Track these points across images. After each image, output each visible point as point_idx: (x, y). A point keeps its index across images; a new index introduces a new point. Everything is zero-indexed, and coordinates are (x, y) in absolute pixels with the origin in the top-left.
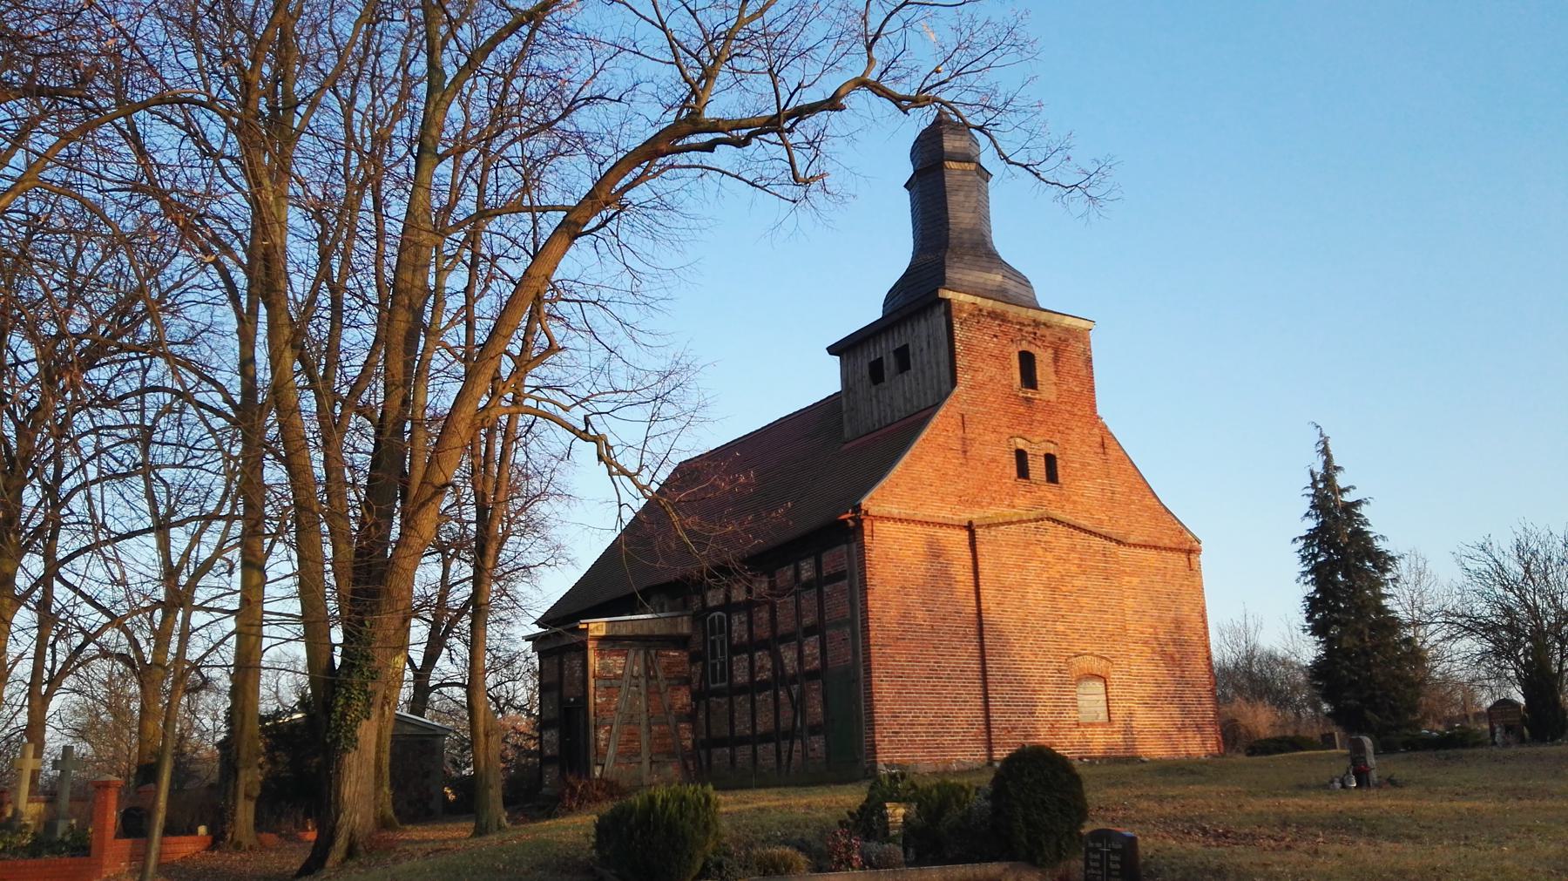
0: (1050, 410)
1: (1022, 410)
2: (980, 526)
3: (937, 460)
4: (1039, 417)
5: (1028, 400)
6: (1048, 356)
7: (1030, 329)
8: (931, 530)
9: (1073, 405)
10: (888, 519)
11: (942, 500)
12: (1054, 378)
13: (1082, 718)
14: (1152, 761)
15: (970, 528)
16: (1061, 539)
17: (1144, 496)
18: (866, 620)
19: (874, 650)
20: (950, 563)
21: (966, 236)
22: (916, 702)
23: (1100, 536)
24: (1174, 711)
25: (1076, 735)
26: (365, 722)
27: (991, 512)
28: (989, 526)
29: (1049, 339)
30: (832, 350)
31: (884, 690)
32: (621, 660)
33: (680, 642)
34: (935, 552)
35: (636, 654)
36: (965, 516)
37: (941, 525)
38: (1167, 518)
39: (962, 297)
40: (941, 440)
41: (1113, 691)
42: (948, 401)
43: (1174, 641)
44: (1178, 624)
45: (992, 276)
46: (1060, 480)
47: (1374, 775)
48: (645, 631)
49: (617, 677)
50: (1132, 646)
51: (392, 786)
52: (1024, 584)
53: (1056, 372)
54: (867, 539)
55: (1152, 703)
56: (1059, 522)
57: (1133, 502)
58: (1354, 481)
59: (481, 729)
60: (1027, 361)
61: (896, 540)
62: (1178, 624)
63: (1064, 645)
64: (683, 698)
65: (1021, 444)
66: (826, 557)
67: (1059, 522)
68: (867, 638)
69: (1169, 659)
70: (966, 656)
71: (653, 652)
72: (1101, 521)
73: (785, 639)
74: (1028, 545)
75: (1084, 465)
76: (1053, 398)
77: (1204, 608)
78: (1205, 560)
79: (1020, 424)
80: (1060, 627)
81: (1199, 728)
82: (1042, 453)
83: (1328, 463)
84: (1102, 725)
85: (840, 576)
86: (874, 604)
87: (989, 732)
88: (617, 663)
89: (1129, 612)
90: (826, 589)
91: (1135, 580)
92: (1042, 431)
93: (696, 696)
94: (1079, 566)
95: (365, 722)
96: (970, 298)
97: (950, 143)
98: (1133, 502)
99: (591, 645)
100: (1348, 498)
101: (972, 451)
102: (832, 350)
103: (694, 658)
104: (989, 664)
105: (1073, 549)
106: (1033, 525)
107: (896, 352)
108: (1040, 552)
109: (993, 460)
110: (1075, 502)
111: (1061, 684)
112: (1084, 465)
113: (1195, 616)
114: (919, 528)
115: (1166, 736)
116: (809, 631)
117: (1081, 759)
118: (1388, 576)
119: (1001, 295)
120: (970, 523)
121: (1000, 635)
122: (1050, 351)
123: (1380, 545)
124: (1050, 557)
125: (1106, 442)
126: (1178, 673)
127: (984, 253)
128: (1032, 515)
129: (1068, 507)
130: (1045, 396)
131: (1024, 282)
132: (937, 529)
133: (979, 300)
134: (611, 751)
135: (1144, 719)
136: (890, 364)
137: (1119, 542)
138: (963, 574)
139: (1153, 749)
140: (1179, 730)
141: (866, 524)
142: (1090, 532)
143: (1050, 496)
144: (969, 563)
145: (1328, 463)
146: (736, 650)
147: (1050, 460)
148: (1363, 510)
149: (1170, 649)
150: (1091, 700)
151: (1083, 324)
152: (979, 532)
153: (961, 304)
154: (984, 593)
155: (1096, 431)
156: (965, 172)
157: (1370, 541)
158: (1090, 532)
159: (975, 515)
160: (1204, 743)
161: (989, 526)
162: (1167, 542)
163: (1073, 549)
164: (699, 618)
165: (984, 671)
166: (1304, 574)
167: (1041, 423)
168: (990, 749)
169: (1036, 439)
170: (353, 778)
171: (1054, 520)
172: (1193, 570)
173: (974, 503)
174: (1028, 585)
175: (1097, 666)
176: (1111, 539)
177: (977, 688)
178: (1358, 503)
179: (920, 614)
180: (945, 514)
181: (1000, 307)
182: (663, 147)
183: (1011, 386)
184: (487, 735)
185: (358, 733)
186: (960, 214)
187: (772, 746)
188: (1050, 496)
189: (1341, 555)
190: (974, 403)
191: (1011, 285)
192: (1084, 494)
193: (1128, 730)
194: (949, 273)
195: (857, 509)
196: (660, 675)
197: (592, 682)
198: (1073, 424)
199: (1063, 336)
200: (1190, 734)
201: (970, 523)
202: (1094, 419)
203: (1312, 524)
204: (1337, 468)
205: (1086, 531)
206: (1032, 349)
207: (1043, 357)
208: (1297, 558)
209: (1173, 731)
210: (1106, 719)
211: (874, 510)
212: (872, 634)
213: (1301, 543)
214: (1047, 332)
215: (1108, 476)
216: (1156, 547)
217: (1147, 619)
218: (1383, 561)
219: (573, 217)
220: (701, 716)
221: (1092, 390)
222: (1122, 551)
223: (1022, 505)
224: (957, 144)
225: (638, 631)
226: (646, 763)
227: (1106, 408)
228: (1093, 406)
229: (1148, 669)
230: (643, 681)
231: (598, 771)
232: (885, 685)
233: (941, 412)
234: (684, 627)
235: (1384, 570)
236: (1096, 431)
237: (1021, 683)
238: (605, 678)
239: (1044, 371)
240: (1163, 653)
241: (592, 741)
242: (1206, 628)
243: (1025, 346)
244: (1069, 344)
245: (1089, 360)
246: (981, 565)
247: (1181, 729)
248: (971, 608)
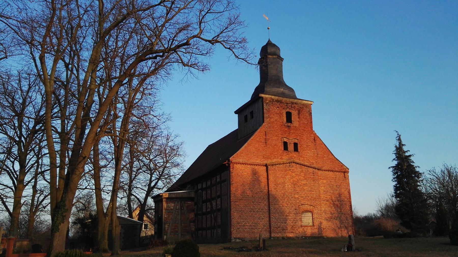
0: (296, 129)
1: (286, 129)
2: (269, 165)
3: (256, 145)
4: (292, 131)
5: (288, 126)
6: (297, 112)
7: (290, 105)
8: (253, 167)
9: (305, 127)
10: (239, 163)
11: (257, 157)
12: (298, 119)
13: (303, 224)
14: (328, 238)
15: (266, 165)
16: (298, 169)
17: (329, 155)
18: (230, 194)
19: (232, 203)
20: (259, 177)
21: (273, 77)
22: (246, 219)
23: (312, 168)
24: (338, 222)
25: (301, 229)
26: (62, 224)
27: (274, 161)
28: (273, 165)
29: (297, 107)
30: (236, 112)
31: (235, 216)
32: (173, 205)
33: (191, 199)
34: (255, 173)
35: (178, 202)
36: (265, 162)
37: (257, 165)
38: (337, 162)
39: (267, 96)
40: (258, 139)
41: (315, 216)
42: (261, 127)
43: (338, 200)
44: (340, 195)
45: (280, 89)
46: (299, 151)
47: (354, 248)
48: (180, 196)
49: (171, 209)
50: (323, 202)
51: (108, 240)
52: (284, 183)
53: (299, 118)
54: (231, 170)
55: (328, 220)
56: (297, 164)
57: (325, 157)
58: (409, 148)
59: (114, 226)
60: (289, 115)
61: (241, 170)
62: (340, 195)
63: (298, 201)
64: (192, 215)
65: (285, 140)
66: (222, 175)
67: (297, 164)
68: (230, 199)
69: (336, 206)
70: (264, 205)
71: (183, 202)
72: (313, 164)
73: (213, 199)
74: (286, 171)
75: (307, 146)
76: (297, 126)
77: (349, 190)
78: (351, 176)
79: (285, 134)
80: (296, 196)
81: (346, 228)
82: (293, 142)
83: (400, 143)
84: (310, 226)
85: (225, 181)
86: (233, 189)
87: (270, 228)
88: (172, 205)
89: (322, 191)
90: (222, 184)
91: (325, 181)
92: (293, 135)
93: (196, 215)
94: (304, 177)
95: (62, 224)
96: (270, 96)
97: (270, 50)
98: (325, 157)
99: (164, 200)
100: (407, 154)
101: (268, 142)
102: (236, 112)
103: (196, 204)
104: (271, 207)
105: (302, 171)
106: (288, 165)
107: (251, 113)
108: (290, 173)
109: (275, 145)
110: (303, 157)
111: (296, 214)
112: (307, 146)
113: (346, 192)
114: (249, 166)
115: (334, 230)
116: (219, 197)
117: (302, 237)
118: (420, 179)
119: (283, 95)
120: (266, 164)
121: (275, 198)
122: (297, 111)
123: (417, 169)
124: (294, 174)
125: (316, 139)
126: (339, 210)
127: (280, 82)
128: (288, 161)
129: (301, 159)
130: (295, 125)
131: (292, 90)
132: (255, 166)
133: (273, 97)
134: (169, 231)
135: (325, 224)
136: (249, 116)
137: (318, 169)
138: (263, 180)
139: (329, 234)
140: (339, 228)
141: (231, 165)
142: (308, 167)
143: (295, 156)
144: (266, 176)
145: (400, 143)
146: (203, 202)
147: (296, 145)
148: (412, 158)
149: (337, 203)
150: (307, 219)
151: (309, 103)
152: (269, 167)
153: (266, 98)
154: (270, 185)
155: (312, 135)
156: (274, 58)
157: (414, 168)
158: (308, 167)
159: (268, 162)
160: (348, 233)
161: (273, 165)
162: (337, 169)
163: (302, 171)
164: (196, 192)
165: (269, 210)
166: (394, 178)
167: (293, 133)
168: (270, 233)
169: (291, 138)
170: (57, 240)
171: (295, 163)
172: (346, 178)
173: (268, 158)
174: (286, 183)
175: (309, 208)
176: (316, 169)
177: (267, 215)
178: (410, 156)
179: (248, 192)
180: (258, 161)
181: (280, 98)
182: (144, 58)
183: (283, 122)
184: (116, 227)
185: (60, 227)
186: (272, 72)
187: (210, 231)
188: (295, 156)
189: (404, 171)
190: (270, 127)
191: (286, 92)
192: (308, 155)
193: (320, 228)
194: (266, 89)
195: (229, 161)
196: (185, 209)
197: (164, 211)
198: (304, 133)
199: (301, 106)
200: (343, 230)
201: (266, 164)
202: (312, 132)
203: (395, 163)
204: (403, 145)
205: (307, 166)
206: (291, 111)
207: (294, 114)
208: (391, 174)
209: (337, 229)
210: (312, 225)
211: (234, 161)
212: (232, 198)
213: (391, 169)
214: (296, 106)
215: (316, 149)
216: (332, 171)
217: (329, 194)
218: (418, 174)
219: (120, 79)
220: (196, 221)
221: (312, 122)
222: (320, 172)
223: (285, 158)
224: (272, 50)
225: (178, 196)
226: (180, 235)
227: (317, 128)
228: (312, 128)
229: (328, 209)
230: (180, 211)
231: (165, 237)
232: (235, 214)
233: (258, 131)
234: (193, 195)
235: (419, 178)
236: (312, 135)
237: (282, 213)
238: (168, 210)
239: (294, 117)
240: (334, 204)
241: (163, 228)
242: (350, 196)
243: (288, 110)
244: (305, 110)
245: (311, 114)
246: (269, 177)
247: (340, 228)
248: (266, 191)
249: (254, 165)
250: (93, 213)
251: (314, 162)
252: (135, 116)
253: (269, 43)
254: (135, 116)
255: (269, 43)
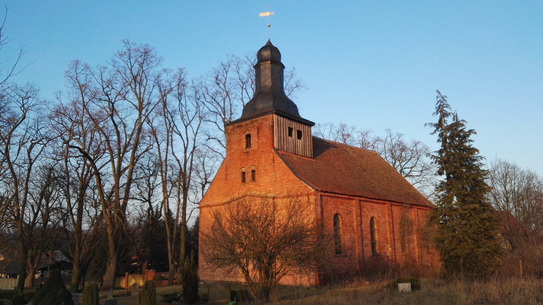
12: (257, 140)
57: (284, 179)
65: (243, 170)
82: (250, 171)
98: (284, 179)
101: (228, 177)
110: (261, 186)
143: (252, 186)
160: (309, 280)
188: (252, 186)
215: (274, 171)
243: (247, 133)
249: (217, 205)
250: (151, 275)
251: (271, 189)
252: (83, 127)
253: (269, 46)
254: (83, 127)
255: (269, 46)
